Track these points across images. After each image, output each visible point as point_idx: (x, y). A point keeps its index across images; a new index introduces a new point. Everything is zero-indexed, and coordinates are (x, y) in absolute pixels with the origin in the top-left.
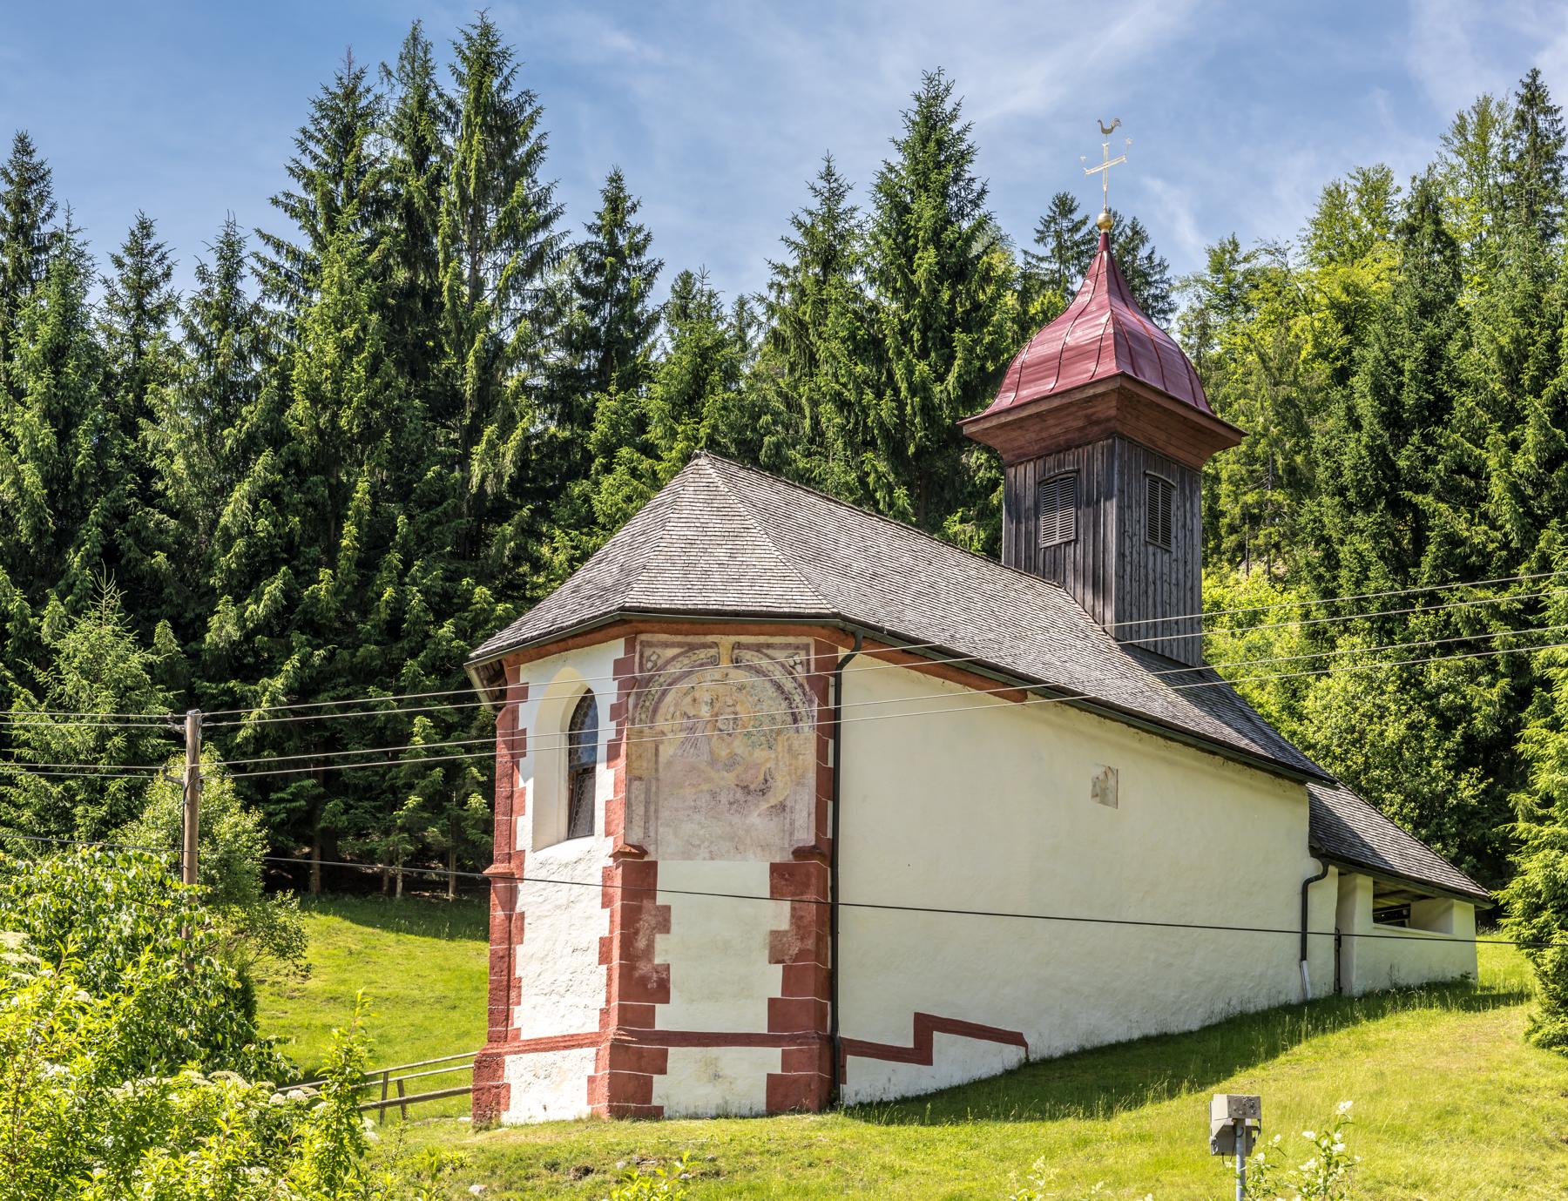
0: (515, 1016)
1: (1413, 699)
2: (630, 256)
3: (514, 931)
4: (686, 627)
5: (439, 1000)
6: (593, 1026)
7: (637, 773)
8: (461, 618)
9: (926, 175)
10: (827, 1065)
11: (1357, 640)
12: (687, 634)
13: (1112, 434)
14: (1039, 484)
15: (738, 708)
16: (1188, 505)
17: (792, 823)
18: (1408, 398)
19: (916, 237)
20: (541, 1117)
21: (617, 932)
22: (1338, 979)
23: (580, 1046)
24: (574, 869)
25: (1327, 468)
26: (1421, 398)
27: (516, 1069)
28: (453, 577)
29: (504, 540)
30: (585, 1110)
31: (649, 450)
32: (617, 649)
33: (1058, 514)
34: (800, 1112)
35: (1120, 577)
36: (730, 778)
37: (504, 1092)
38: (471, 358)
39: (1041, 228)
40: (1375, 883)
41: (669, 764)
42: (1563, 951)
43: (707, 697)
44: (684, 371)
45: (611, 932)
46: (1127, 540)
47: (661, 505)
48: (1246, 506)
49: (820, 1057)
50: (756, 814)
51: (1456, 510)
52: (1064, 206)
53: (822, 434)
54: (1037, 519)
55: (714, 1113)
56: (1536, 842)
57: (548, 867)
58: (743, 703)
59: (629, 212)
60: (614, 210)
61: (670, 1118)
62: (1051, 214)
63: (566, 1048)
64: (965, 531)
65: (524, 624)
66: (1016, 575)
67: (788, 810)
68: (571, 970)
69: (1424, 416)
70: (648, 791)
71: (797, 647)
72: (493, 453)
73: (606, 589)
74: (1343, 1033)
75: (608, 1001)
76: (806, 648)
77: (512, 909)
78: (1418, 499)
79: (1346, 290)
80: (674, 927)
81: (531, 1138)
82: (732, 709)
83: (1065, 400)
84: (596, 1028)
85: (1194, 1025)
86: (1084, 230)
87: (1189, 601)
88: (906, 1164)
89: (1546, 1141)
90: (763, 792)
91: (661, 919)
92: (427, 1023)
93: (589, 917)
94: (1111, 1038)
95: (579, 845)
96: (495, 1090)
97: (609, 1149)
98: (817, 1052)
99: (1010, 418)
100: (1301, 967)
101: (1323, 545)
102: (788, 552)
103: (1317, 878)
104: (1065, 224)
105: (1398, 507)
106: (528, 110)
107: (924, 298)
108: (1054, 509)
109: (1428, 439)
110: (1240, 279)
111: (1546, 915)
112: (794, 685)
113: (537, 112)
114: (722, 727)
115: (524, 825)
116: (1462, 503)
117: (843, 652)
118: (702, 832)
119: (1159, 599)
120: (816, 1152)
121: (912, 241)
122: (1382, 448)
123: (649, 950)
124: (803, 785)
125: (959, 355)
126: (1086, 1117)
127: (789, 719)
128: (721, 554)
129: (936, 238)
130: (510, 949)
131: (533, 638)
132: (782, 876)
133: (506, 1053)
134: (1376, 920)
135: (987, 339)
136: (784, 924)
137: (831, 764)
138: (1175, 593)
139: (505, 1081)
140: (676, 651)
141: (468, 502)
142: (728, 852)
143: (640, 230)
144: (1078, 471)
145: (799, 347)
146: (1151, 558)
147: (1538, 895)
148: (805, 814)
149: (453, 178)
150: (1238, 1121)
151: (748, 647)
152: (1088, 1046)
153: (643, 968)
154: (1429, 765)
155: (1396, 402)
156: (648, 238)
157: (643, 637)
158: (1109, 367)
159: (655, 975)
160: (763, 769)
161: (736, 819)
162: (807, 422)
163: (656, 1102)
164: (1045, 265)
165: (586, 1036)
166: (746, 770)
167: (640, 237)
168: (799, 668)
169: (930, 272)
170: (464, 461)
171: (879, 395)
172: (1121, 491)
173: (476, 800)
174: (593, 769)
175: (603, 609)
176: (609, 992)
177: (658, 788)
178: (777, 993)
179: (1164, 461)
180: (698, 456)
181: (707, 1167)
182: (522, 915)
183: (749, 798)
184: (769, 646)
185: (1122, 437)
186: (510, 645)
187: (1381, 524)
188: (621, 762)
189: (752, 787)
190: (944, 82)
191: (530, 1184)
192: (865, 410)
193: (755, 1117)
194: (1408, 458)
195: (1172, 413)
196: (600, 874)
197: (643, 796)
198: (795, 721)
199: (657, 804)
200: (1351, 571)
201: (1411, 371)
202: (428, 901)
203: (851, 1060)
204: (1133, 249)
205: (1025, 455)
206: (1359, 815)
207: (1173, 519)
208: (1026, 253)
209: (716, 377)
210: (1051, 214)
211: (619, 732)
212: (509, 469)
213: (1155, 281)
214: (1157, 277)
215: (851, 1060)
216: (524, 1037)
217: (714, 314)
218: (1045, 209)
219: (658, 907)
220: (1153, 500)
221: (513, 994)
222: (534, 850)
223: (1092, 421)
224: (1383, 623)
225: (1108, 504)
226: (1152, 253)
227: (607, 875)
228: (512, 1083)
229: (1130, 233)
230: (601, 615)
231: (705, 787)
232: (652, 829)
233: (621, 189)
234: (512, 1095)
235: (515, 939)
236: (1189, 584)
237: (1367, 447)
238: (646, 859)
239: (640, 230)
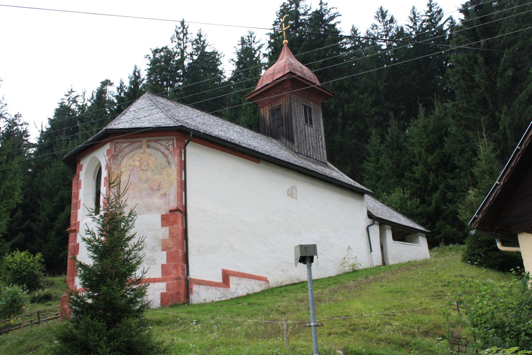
15: (149, 162)
22: (383, 260)
36: (146, 186)
67: (167, 195)
82: (147, 162)
90: (158, 190)
103: (371, 225)
112: (169, 152)
119: (310, 142)
127: (167, 164)
137: (183, 179)
140: (127, 144)
146: (307, 129)
148: (173, 196)
160: (158, 182)
168: (170, 147)
178: (164, 262)
183: (153, 192)
189: (154, 188)
198: (169, 164)
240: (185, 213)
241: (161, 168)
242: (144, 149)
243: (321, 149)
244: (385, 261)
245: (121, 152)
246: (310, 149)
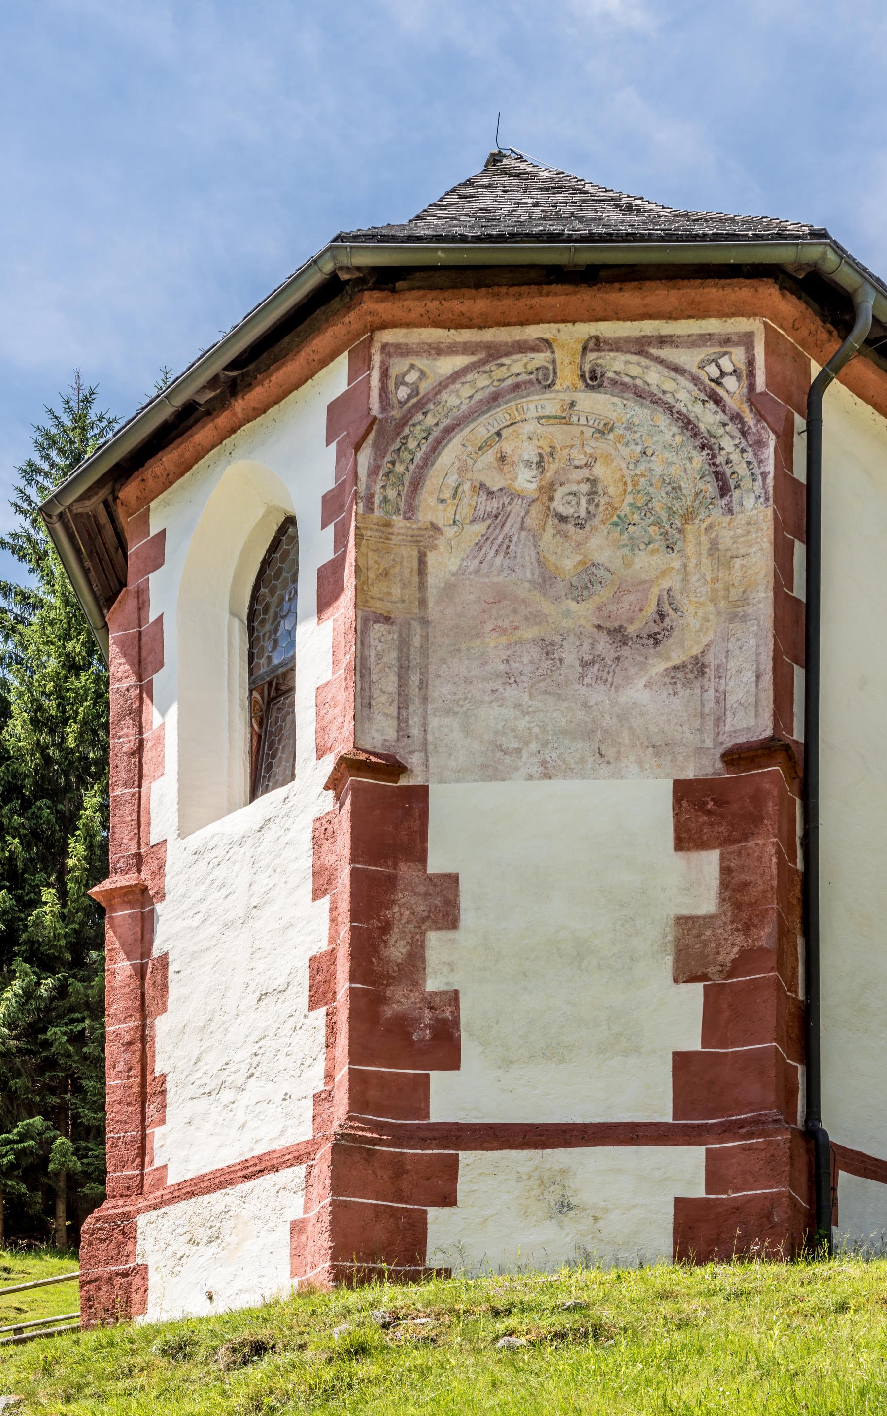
0: (156, 1145)
3: (149, 991)
7: (380, 607)
15: (599, 470)
23: (275, 1168)
37: (137, 1281)
41: (449, 590)
43: (530, 452)
45: (332, 939)
50: (640, 683)
57: (208, 856)
58: (608, 459)
67: (710, 672)
68: (254, 1038)
70: (404, 644)
71: (727, 341)
75: (329, 1076)
77: (146, 953)
80: (467, 916)
90: (656, 639)
91: (438, 901)
96: (118, 1281)
98: (784, 1148)
112: (721, 417)
118: (523, 724)
124: (744, 618)
127: (710, 488)
130: (143, 1027)
132: (700, 806)
133: (139, 1211)
139: (139, 1261)
140: (460, 361)
142: (582, 761)
148: (749, 676)
151: (616, 346)
157: (388, 336)
159: (427, 1014)
160: (655, 592)
161: (598, 695)
166: (620, 592)
168: (731, 383)
176: (331, 1060)
177: (426, 638)
178: (693, 1043)
182: (164, 961)
183: (626, 651)
184: (663, 341)
188: (346, 601)
189: (631, 630)
197: (394, 654)
198: (724, 490)
199: (424, 671)
211: (340, 541)
219: (430, 879)
221: (151, 1109)
222: (182, 834)
228: (151, 1261)
231: (530, 633)
232: (415, 722)
234: (150, 1283)
235: (151, 1008)
238: (403, 782)
242: (567, 397)
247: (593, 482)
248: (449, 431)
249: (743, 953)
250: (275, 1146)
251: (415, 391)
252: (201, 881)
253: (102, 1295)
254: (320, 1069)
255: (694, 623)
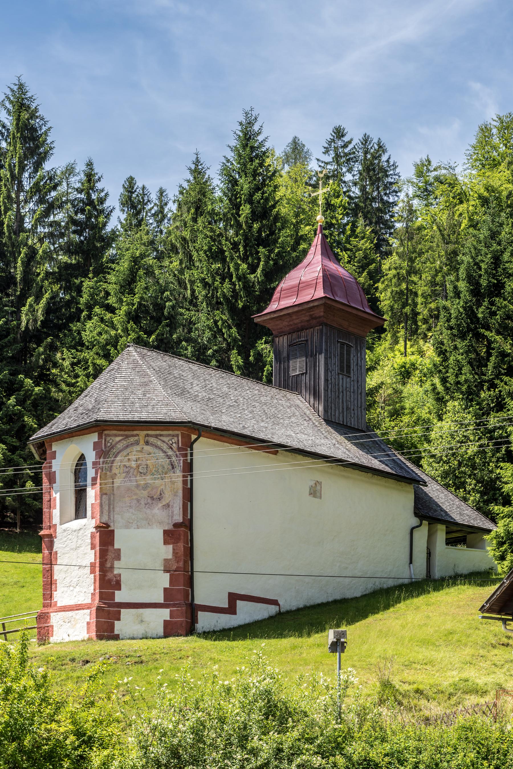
1: (482, 433)
2: (99, 205)
4: (124, 428)
5: (16, 583)
6: (88, 601)
7: (104, 492)
8: (18, 394)
9: (245, 165)
10: (189, 615)
11: (456, 403)
12: (125, 430)
13: (321, 324)
14: (289, 346)
16: (359, 355)
17: (172, 512)
18: (484, 283)
19: (241, 198)
20: (67, 639)
21: (98, 560)
23: (83, 609)
24: (78, 533)
25: (445, 316)
26: (490, 282)
27: (55, 619)
28: (14, 373)
29: (40, 354)
30: (86, 636)
31: (111, 309)
32: (94, 437)
33: (298, 360)
34: (178, 636)
35: (326, 390)
36: (145, 493)
37: (50, 629)
38: (19, 262)
39: (326, 145)
40: (446, 527)
41: (119, 487)
42: (512, 562)
43: (134, 458)
44: (126, 270)
45: (95, 560)
46: (329, 373)
47: (113, 370)
48: (431, 310)
49: (186, 613)
51: (506, 339)
52: (339, 133)
53: (196, 298)
54: (289, 362)
55: (141, 636)
56: (502, 515)
59: (97, 181)
60: (89, 181)
61: (122, 639)
62: (332, 138)
63: (77, 610)
64: (266, 348)
65: (53, 425)
66: (278, 390)
69: (491, 291)
70: (109, 499)
71: (173, 436)
72: (32, 310)
73: (88, 410)
74: (421, 598)
75: (95, 590)
76: (177, 436)
77: (52, 550)
78: (487, 333)
79: (487, 189)
81: (63, 648)
83: (300, 308)
84: (89, 601)
85: (358, 594)
86: (350, 146)
87: (359, 399)
88: (221, 657)
89: (492, 644)
90: (160, 499)
92: (11, 594)
93: (85, 554)
94: (319, 601)
95: (81, 522)
97: (97, 652)
99: (275, 315)
100: (410, 567)
101: (442, 356)
102: (169, 391)
103: (417, 527)
104: (340, 143)
105: (478, 337)
106: (44, 129)
107: (244, 230)
108: (297, 358)
109: (492, 303)
110: (432, 180)
111: (505, 546)
113: (49, 129)
114: (142, 471)
115: (56, 513)
116: (509, 335)
117: (194, 437)
118: (133, 517)
119: (345, 400)
120: (183, 653)
121: (238, 200)
122: (471, 307)
123: (112, 568)
124: (177, 496)
125: (262, 260)
126: (299, 637)
127: (170, 467)
128: (139, 393)
129: (250, 201)
131: (57, 432)
132: (168, 535)
134: (447, 544)
135: (276, 250)
136: (170, 556)
137: (189, 486)
138: (352, 396)
140: (120, 438)
141: (20, 334)
143: (102, 190)
144: (307, 341)
145: (184, 253)
146: (341, 381)
147: (503, 538)
148: (178, 508)
149: (7, 166)
150: (338, 640)
151: (151, 436)
152: (308, 605)
153: (109, 576)
154: (489, 465)
155: (478, 284)
156: (107, 195)
157: (106, 432)
158: (320, 293)
161: (148, 511)
162: (189, 292)
163: (116, 632)
164: (329, 167)
165: (86, 605)
167: (103, 194)
168: (174, 445)
169: (247, 218)
170: (17, 314)
171: (223, 280)
172: (326, 350)
173: (29, 485)
174: (86, 489)
175: (88, 420)
176: (95, 586)
178: (168, 586)
179: (347, 335)
180: (129, 346)
181: (137, 659)
182: (56, 552)
184: (161, 435)
185: (326, 325)
186: (48, 435)
187: (469, 346)
188: (98, 486)
189: (155, 497)
190: (254, 115)
191: (64, 667)
192: (216, 289)
193: (159, 638)
194: (482, 312)
195: (350, 313)
196: (90, 535)
198: (173, 468)
200: (454, 370)
201: (485, 269)
202: (8, 534)
203: (200, 614)
204: (379, 157)
205: (283, 332)
206: (442, 495)
207: (352, 361)
208: (318, 160)
209: (141, 272)
210: (332, 138)
211: (96, 473)
212: (40, 315)
213: (391, 174)
214: (392, 172)
215: (200, 614)
216: (59, 605)
217: (146, 198)
218: (328, 134)
219: (115, 550)
220: (342, 354)
221: (53, 587)
222: (61, 524)
223: (312, 318)
224: (468, 395)
225: (320, 356)
226: (389, 158)
227: (93, 536)
228: (54, 625)
229: (376, 147)
230: (87, 423)
231: (134, 497)
232: (112, 516)
233: (92, 169)
236: (360, 391)
237: (463, 307)
239: (102, 190)
240: (191, 527)
241: (163, 472)
242: (142, 446)
243: (359, 409)
244: (431, 573)
245: (112, 448)
246: (343, 412)
247: (147, 465)
248: (118, 453)
249: (177, 567)
250: (83, 603)
251: (111, 444)
252: (65, 537)
253: (42, 631)
254: (92, 588)
255: (167, 496)
